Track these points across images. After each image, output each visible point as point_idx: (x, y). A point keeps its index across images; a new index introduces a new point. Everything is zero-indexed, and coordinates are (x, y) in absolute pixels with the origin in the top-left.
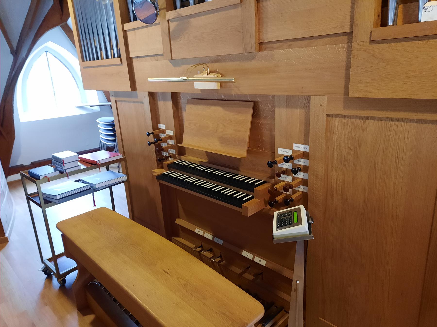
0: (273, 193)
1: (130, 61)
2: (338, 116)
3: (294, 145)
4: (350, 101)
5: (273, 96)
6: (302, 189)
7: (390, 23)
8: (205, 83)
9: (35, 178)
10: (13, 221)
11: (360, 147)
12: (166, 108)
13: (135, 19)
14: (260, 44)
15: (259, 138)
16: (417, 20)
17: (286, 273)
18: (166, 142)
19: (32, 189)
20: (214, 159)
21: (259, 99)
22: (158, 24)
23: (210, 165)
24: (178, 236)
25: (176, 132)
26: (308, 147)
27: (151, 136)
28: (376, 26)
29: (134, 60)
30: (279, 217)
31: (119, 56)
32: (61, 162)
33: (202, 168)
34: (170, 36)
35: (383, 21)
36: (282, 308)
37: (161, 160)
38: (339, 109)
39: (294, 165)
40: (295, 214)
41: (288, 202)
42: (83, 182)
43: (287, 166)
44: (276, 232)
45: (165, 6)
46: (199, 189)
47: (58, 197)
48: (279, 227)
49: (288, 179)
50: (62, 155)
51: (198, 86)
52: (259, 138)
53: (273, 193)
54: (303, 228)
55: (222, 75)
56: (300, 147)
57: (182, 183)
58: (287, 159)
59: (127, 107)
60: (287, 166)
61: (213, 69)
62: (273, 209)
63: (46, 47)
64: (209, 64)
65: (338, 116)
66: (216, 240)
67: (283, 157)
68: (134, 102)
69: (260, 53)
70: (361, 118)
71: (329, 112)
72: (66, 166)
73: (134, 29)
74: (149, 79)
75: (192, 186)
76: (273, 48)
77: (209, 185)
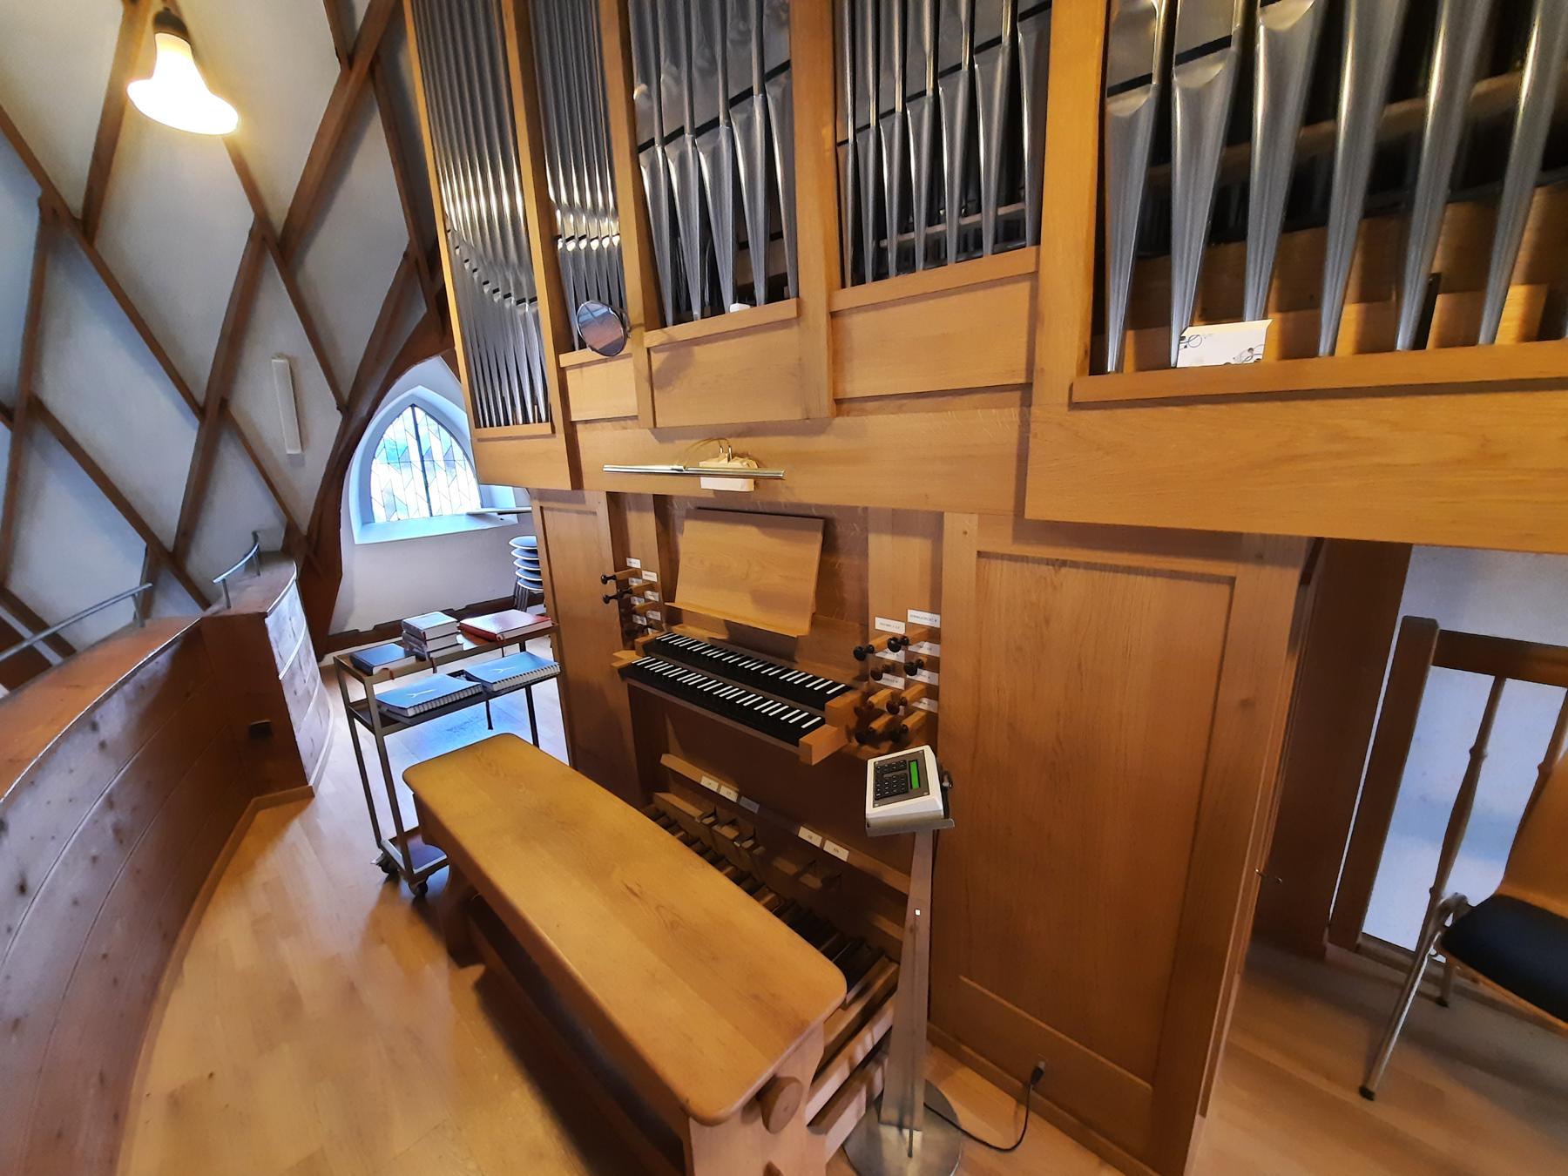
0: (866, 713)
1: (571, 428)
2: (1002, 557)
3: (910, 612)
4: (1026, 529)
5: (866, 509)
6: (925, 704)
7: (1110, 367)
8: (724, 475)
9: (362, 671)
10: (328, 751)
11: (1047, 622)
12: (643, 526)
13: (583, 346)
14: (838, 402)
15: (837, 597)
16: (1165, 364)
17: (892, 878)
18: (642, 595)
19: (357, 692)
20: (741, 637)
21: (834, 514)
22: (629, 355)
23: (732, 648)
24: (666, 791)
25: (662, 576)
26: (937, 617)
27: (611, 583)
28: (1080, 373)
29: (579, 427)
30: (879, 770)
31: (549, 418)
32: (419, 636)
33: (716, 654)
34: (653, 382)
35: (1095, 362)
36: (882, 952)
37: (630, 634)
38: (1004, 543)
39: (909, 655)
40: (914, 765)
41: (898, 737)
42: (469, 678)
43: (897, 657)
44: (875, 812)
45: (642, 320)
46: (709, 700)
47: (411, 713)
48: (880, 798)
49: (898, 683)
50: (420, 622)
51: (708, 484)
52: (837, 597)
53: (866, 713)
54: (930, 803)
55: (760, 464)
56: (922, 618)
57: (673, 686)
58: (896, 643)
59: (563, 523)
60: (897, 657)
61: (741, 450)
62: (866, 748)
63: (412, 396)
64: (731, 440)
65: (1002, 557)
66: (745, 802)
67: (886, 638)
68: (579, 512)
69: (838, 420)
70: (1049, 562)
71: (982, 549)
72: (430, 646)
73: (581, 365)
74: (608, 468)
75: (692, 693)
76: (864, 412)
77: (729, 692)
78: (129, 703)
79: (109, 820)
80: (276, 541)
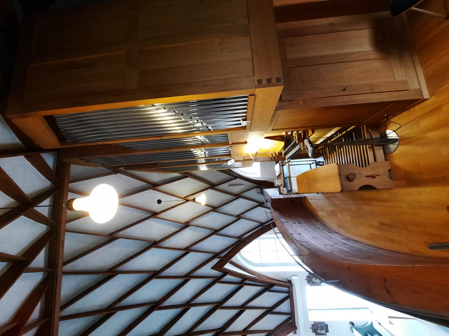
78: (281, 218)
79: (297, 224)
80: (259, 190)
